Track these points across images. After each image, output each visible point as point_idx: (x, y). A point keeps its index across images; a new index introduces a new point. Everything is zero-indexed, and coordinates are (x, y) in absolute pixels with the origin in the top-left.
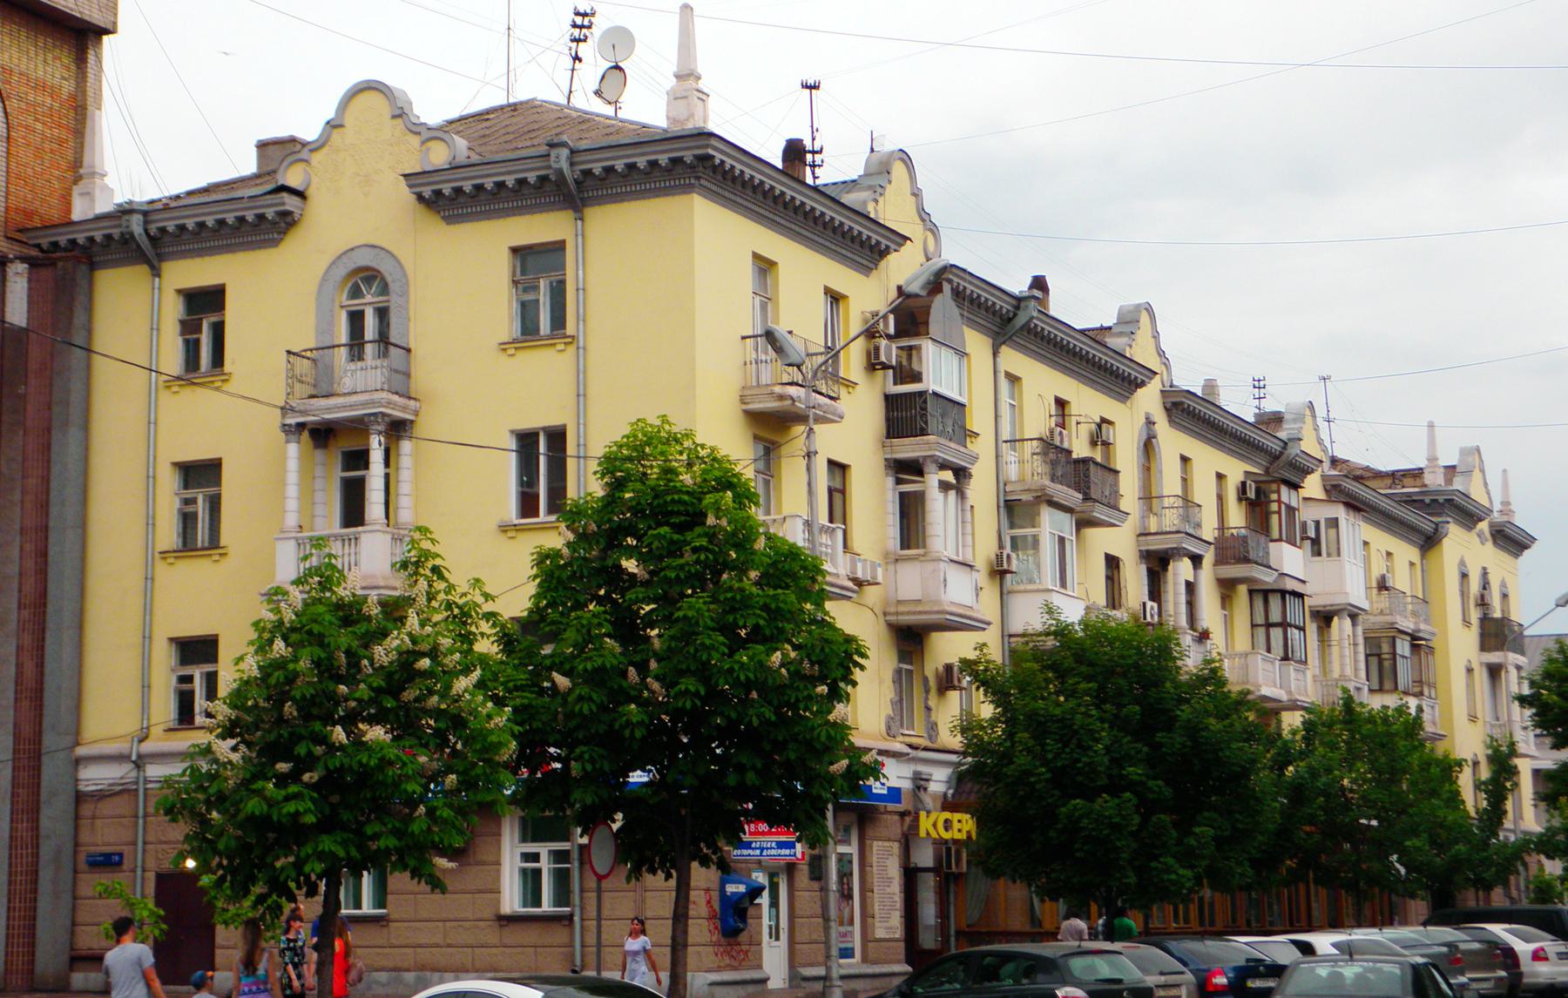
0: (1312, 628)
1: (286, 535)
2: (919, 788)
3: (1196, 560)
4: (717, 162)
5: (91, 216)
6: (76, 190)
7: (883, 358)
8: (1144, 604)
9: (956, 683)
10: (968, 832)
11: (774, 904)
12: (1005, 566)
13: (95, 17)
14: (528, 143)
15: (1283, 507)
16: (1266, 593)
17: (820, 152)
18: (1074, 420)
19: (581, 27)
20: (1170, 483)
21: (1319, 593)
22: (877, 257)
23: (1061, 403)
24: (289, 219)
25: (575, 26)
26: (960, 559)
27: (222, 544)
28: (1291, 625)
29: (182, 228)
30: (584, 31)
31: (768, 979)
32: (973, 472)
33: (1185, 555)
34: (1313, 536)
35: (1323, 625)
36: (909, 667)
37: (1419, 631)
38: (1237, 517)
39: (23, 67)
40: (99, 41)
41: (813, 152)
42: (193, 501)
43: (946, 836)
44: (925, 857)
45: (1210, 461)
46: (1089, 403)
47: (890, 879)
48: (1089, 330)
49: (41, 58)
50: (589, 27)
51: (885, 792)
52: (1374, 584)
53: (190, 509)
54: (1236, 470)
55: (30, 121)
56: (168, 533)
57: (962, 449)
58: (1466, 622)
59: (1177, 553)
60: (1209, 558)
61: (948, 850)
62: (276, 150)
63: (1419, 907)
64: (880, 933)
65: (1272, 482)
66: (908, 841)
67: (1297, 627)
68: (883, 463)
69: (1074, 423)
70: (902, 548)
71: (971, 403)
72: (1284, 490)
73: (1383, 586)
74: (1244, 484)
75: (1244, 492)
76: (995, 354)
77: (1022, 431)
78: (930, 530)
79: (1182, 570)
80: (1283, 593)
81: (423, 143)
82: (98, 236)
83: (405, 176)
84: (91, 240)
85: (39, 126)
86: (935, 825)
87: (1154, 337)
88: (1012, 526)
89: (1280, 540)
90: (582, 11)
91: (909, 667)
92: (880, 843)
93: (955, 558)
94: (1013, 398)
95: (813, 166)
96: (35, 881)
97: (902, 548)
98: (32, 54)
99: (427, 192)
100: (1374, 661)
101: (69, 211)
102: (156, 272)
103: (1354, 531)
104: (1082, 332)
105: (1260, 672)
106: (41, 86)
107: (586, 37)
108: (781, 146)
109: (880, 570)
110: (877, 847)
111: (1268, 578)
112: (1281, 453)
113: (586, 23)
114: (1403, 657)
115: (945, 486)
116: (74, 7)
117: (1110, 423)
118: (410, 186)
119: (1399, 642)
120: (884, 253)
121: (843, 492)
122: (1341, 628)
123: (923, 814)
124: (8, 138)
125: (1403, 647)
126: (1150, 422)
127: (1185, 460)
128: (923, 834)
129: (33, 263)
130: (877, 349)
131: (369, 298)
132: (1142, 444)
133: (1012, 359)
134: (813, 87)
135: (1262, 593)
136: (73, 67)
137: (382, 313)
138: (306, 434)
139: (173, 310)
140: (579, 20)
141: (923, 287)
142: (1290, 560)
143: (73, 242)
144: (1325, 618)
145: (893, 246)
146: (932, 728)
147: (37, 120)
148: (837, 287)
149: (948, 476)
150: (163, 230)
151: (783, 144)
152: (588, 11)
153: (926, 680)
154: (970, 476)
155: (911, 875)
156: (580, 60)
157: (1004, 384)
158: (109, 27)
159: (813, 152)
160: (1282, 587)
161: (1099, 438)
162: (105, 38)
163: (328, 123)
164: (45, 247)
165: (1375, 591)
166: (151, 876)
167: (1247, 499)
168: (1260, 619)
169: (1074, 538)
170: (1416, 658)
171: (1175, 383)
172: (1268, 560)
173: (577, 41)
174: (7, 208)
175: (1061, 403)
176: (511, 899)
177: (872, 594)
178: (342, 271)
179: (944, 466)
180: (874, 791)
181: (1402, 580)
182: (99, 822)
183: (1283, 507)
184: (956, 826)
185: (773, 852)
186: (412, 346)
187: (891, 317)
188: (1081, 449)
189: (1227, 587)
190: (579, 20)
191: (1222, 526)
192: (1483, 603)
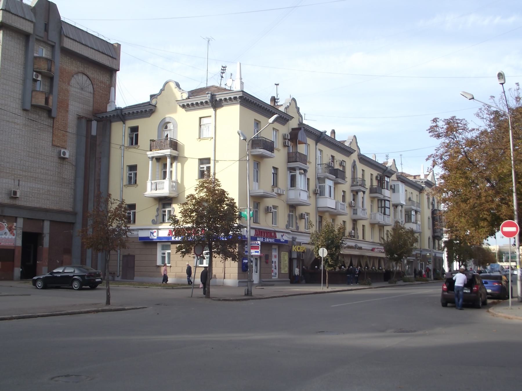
0: (392, 209)
2: (293, 240)
3: (364, 192)
4: (245, 98)
5: (111, 110)
6: (108, 105)
7: (287, 144)
8: (351, 202)
9: (303, 217)
10: (304, 250)
11: (256, 265)
12: (317, 192)
13: (114, 67)
15: (386, 181)
16: (381, 200)
17: (279, 99)
18: (336, 160)
19: (223, 70)
20: (359, 175)
21: (394, 201)
22: (286, 121)
24: (152, 111)
25: (222, 70)
26: (304, 190)
27: (137, 184)
28: (387, 207)
29: (129, 113)
30: (224, 71)
31: (253, 281)
32: (308, 170)
33: (361, 191)
34: (393, 188)
35: (395, 207)
36: (292, 214)
37: (417, 209)
38: (375, 183)
39: (98, 78)
41: (277, 99)
42: (131, 174)
43: (298, 251)
44: (295, 256)
45: (369, 171)
46: (339, 157)
47: (286, 261)
48: (341, 141)
49: (102, 76)
50: (225, 70)
51: (284, 241)
52: (408, 199)
53: (131, 176)
54: (375, 173)
55: (99, 90)
56: (126, 181)
57: (305, 165)
58: (429, 208)
59: (360, 191)
60: (367, 192)
61: (300, 254)
62: (152, 97)
63: (508, 260)
64: (283, 272)
65: (384, 176)
66: (290, 252)
67: (388, 208)
68: (287, 168)
69: (336, 161)
70: (291, 187)
71: (346, 166)
72: (386, 178)
73: (410, 199)
74: (377, 176)
75: (377, 178)
76: (316, 145)
77: (323, 162)
78: (297, 183)
79: (360, 194)
80: (385, 200)
81: (181, 94)
82: (112, 115)
84: (110, 116)
85: (101, 91)
86: (296, 249)
87: (356, 143)
88: (319, 183)
89: (385, 189)
90: (223, 66)
91: (292, 214)
92: (283, 252)
93: (303, 189)
94: (321, 155)
95: (277, 102)
96: (97, 257)
97: (291, 187)
98: (100, 75)
99: (181, 104)
100: (407, 216)
101: (107, 110)
102: (124, 123)
103: (402, 187)
104: (339, 142)
105: (386, 219)
106: (102, 82)
109: (284, 192)
110: (282, 253)
111: (381, 197)
112: (386, 170)
113: (224, 69)
114: (413, 215)
115: (300, 174)
116: (109, 65)
119: (412, 212)
120: (288, 121)
121: (276, 174)
122: (399, 208)
123: (293, 246)
124: (94, 93)
125: (413, 213)
126: (354, 162)
127: (363, 170)
128: (293, 250)
129: (98, 121)
130: (285, 142)
132: (352, 167)
133: (320, 146)
135: (380, 200)
136: (110, 78)
138: (154, 159)
139: (128, 131)
140: (223, 68)
142: (387, 193)
143: (107, 116)
144: (396, 206)
145: (290, 119)
146: (298, 228)
147: (101, 90)
149: (302, 171)
150: (125, 113)
151: (271, 97)
152: (225, 66)
153: (296, 217)
154: (307, 171)
155: (291, 260)
156: (223, 77)
157: (318, 153)
158: (117, 69)
159: (277, 99)
160: (385, 199)
161: (342, 164)
163: (161, 89)
164: (101, 118)
165: (408, 201)
166: (121, 256)
167: (378, 180)
168: (380, 206)
170: (416, 215)
171: (361, 153)
172: (382, 193)
173: (222, 73)
174: (93, 109)
177: (283, 197)
179: (300, 169)
180: (281, 240)
181: (414, 199)
182: (422, 248)
183: (386, 181)
184: (301, 249)
185: (254, 253)
188: (337, 166)
189: (372, 199)
190: (223, 68)
191: (372, 185)
192: (433, 205)
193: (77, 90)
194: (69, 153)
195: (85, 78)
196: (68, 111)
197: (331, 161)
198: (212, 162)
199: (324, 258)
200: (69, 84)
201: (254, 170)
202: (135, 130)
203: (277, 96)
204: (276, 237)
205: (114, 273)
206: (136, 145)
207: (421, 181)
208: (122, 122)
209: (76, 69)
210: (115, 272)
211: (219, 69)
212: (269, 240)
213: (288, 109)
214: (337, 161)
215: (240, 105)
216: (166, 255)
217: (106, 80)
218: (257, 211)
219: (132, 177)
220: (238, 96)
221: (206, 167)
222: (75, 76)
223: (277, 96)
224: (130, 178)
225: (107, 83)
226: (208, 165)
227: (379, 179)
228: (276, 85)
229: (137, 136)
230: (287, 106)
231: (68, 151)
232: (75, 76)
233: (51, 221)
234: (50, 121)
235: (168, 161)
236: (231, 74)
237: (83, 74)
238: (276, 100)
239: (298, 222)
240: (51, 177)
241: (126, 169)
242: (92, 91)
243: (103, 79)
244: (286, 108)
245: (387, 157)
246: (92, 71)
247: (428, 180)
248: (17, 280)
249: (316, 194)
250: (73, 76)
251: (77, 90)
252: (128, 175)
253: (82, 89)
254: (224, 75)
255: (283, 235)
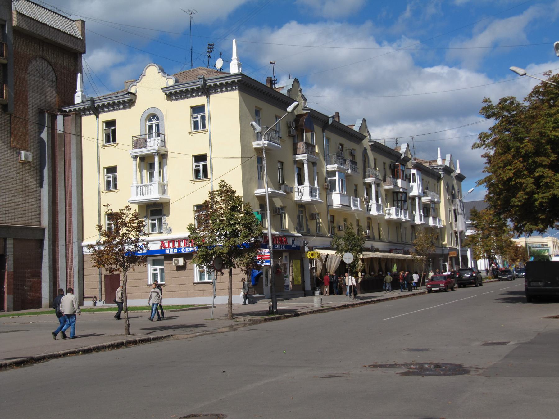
1: (133, 185)
13: (80, 49)
14: (195, 79)
17: (276, 80)
19: (210, 48)
23: (341, 145)
24: (132, 102)
25: (208, 48)
36: (302, 214)
40: (81, 57)
41: (274, 80)
53: (109, 179)
74: (391, 165)
81: (166, 79)
83: (162, 88)
90: (210, 44)
91: (302, 214)
94: (328, 143)
95: (274, 84)
98: (62, 59)
99: (167, 92)
100: (425, 209)
102: (97, 117)
107: (212, 51)
108: (265, 79)
117: (354, 150)
118: (163, 91)
124: (57, 82)
130: (290, 131)
131: (154, 122)
134: (274, 63)
137: (158, 126)
139: (102, 126)
140: (210, 47)
141: (485, 199)
147: (64, 77)
148: (342, 143)
158: (82, 51)
159: (274, 80)
162: (83, 55)
168: (395, 199)
169: (345, 180)
175: (341, 145)
176: (197, 279)
178: (146, 115)
186: (165, 134)
187: (294, 123)
190: (210, 47)
193: (36, 79)
194: (518, 104)
195: (45, 63)
196: (27, 105)
197: (340, 150)
198: (208, 159)
199: (350, 265)
200: (26, 71)
201: (258, 166)
202: (111, 124)
203: (274, 77)
204: (286, 243)
205: (95, 297)
206: (114, 143)
207: (438, 168)
208: (94, 116)
209: (33, 53)
210: (96, 296)
211: (205, 49)
212: (280, 247)
213: (290, 92)
214: (346, 150)
215: (239, 90)
216: (158, 271)
217: (70, 65)
218: (264, 213)
219: (110, 181)
220: (236, 80)
221: (202, 165)
222: (33, 62)
223: (274, 77)
224: (109, 183)
225: (72, 69)
226: (204, 163)
227: (393, 168)
228: (272, 64)
229: (114, 132)
230: (289, 89)
231: (31, 153)
232: (33, 62)
233: (15, 239)
234: (7, 117)
235: (156, 160)
236: (220, 53)
237: (43, 58)
238: (273, 82)
239: (309, 223)
240: (12, 185)
241: (103, 172)
242: (54, 79)
243: (66, 64)
244: (289, 91)
245: (396, 144)
246: (53, 55)
247: (446, 166)
248: (427, 294)
249: (326, 189)
250: (30, 62)
251: (36, 79)
252: (106, 179)
253: (42, 77)
254: (211, 55)
255: (295, 240)
